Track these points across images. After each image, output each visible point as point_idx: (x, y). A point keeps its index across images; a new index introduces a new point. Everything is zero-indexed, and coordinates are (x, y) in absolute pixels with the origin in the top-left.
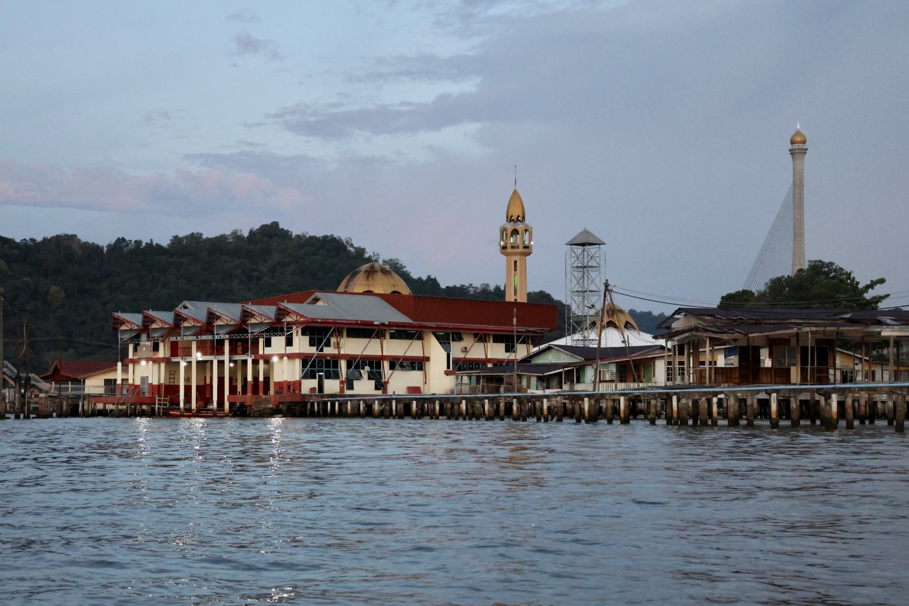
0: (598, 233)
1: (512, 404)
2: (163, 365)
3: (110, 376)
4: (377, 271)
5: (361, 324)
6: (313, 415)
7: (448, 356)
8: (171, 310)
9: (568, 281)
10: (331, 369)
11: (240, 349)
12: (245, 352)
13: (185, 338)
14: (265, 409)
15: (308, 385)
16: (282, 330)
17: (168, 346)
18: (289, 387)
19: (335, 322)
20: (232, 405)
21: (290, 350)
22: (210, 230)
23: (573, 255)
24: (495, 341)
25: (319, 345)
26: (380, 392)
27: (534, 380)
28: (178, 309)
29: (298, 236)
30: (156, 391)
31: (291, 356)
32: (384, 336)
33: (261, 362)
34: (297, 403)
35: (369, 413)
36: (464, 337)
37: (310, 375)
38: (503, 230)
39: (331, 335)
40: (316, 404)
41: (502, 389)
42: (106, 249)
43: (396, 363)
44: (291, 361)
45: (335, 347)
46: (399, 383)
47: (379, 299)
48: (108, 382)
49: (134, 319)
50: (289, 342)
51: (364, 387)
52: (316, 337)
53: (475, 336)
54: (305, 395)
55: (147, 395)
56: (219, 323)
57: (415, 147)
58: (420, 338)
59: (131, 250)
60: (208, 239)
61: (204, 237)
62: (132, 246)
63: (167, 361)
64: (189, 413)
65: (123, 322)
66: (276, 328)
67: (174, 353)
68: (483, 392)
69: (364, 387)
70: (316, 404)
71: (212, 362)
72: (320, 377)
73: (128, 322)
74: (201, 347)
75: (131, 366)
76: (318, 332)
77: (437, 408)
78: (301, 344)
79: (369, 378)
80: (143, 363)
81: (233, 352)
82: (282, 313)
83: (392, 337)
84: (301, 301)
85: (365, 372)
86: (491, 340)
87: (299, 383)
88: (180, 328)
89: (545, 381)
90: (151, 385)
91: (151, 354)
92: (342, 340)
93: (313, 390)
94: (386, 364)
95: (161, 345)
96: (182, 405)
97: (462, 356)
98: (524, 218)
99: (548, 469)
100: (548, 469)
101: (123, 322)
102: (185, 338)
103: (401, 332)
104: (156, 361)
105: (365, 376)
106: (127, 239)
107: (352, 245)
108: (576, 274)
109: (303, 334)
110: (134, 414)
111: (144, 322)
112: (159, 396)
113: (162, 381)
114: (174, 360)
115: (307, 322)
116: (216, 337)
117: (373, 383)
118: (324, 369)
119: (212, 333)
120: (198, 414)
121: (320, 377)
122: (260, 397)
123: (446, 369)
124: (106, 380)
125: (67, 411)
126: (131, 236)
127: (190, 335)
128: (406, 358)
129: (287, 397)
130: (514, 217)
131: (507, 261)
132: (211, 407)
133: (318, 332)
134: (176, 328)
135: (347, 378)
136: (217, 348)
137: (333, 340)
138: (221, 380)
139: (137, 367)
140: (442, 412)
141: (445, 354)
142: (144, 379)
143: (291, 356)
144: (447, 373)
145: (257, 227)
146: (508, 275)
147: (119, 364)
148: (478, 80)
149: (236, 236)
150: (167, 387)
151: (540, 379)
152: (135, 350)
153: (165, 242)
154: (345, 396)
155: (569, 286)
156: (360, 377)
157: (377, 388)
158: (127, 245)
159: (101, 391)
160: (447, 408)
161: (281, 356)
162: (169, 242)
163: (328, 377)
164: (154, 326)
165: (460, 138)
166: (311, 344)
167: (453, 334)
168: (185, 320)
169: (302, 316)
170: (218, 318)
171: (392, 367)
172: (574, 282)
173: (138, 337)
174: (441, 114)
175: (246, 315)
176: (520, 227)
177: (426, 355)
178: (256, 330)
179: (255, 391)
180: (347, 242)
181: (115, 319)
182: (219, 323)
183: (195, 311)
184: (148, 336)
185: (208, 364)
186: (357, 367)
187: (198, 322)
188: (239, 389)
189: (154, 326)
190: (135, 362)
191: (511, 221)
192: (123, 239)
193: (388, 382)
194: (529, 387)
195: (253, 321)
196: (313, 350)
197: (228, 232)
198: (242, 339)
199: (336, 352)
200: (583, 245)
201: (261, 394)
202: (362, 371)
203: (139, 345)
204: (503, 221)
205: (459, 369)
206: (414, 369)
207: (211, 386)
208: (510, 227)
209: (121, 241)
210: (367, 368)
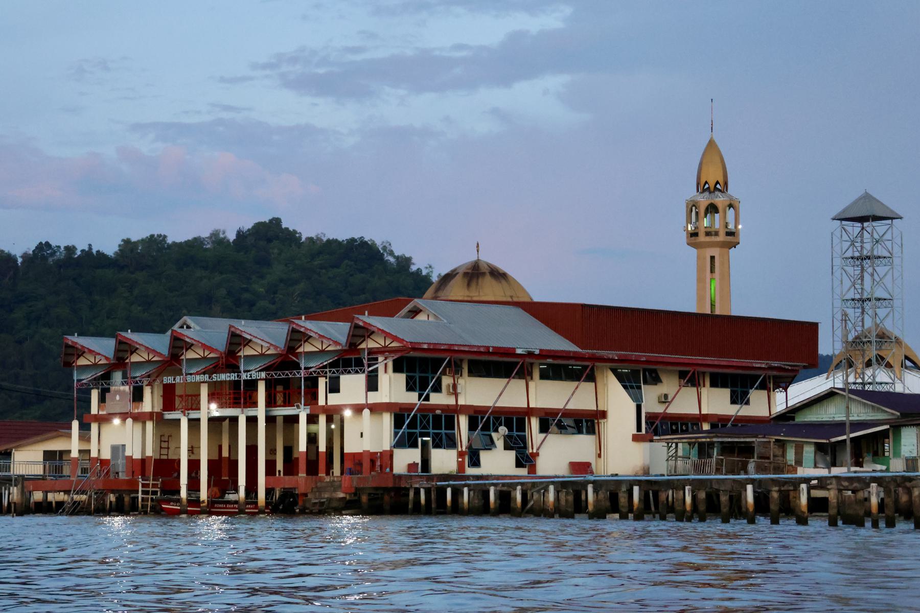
0: (890, 201)
1: (488, 492)
2: (150, 425)
3: (56, 445)
4: (483, 274)
5: (493, 354)
6: (418, 510)
7: (639, 408)
8: (163, 331)
9: (837, 283)
10: (443, 431)
11: (280, 399)
12: (287, 403)
13: (189, 378)
14: (330, 500)
15: (405, 459)
16: (359, 363)
17: (159, 391)
18: (373, 462)
19: (450, 350)
20: (269, 492)
21: (375, 398)
22: (178, 233)
23: (845, 237)
24: (714, 384)
25: (423, 388)
26: (523, 472)
27: (809, 452)
28: (176, 327)
29: (310, 239)
30: (138, 469)
31: (376, 409)
32: (531, 374)
33: (322, 419)
34: (386, 490)
35: (505, 507)
36: (663, 378)
38: (692, 206)
39: (443, 373)
40: (422, 492)
41: (751, 466)
42: (20, 260)
43: (550, 421)
44: (376, 418)
45: (449, 393)
46: (556, 455)
47: (520, 311)
48: (49, 456)
49: (102, 348)
50: (372, 385)
51: (498, 462)
52: (417, 375)
53: (682, 375)
54: (400, 477)
55: (122, 476)
56: (248, 351)
57: (469, 112)
58: (591, 378)
59: (59, 260)
60: (174, 244)
61: (170, 240)
62: (61, 255)
63: (157, 418)
64: (195, 508)
65: (81, 352)
66: (349, 359)
67: (169, 404)
68: (718, 471)
69: (498, 462)
70: (422, 492)
71: (234, 420)
72: (425, 444)
73: (91, 351)
75: (94, 427)
76: (421, 366)
77: (688, 499)
78: (393, 388)
79: (507, 447)
80: (117, 421)
81: (271, 402)
82: (365, 332)
83: (544, 376)
84: (390, 312)
85: (499, 436)
86: (708, 383)
87: (388, 456)
88: (179, 362)
89: (829, 453)
90: (130, 459)
91: (129, 407)
92: (461, 382)
93: (412, 466)
94: (535, 423)
95: (147, 392)
96: (184, 493)
97: (659, 409)
98: (726, 184)
101: (81, 352)
103: (558, 369)
104: (139, 418)
105: (500, 443)
106: (53, 243)
107: (391, 253)
108: (850, 270)
109: (397, 369)
110: (102, 510)
111: (117, 351)
112: (143, 474)
113: (149, 453)
114: (169, 416)
116: (244, 376)
117: (512, 454)
118: (431, 431)
119: (235, 368)
120: (211, 509)
121: (425, 444)
122: (321, 480)
123: (635, 432)
124: (45, 452)
125: (495, 508)
126: (59, 241)
127: (197, 373)
128: (567, 413)
129: (369, 479)
130: (712, 184)
131: (698, 257)
132: (231, 497)
133: (421, 366)
134: (172, 361)
135: (470, 447)
136: (241, 394)
137: (446, 381)
138: (252, 451)
139: (106, 429)
140: (762, 505)
141: (633, 406)
142: (117, 450)
143: (376, 409)
144: (636, 438)
146: (700, 280)
147: (75, 424)
148: (568, 10)
149: (217, 239)
150: (158, 462)
151: (820, 448)
152: (102, 399)
153: (110, 248)
154: (468, 477)
155: (838, 291)
156: (490, 445)
157: (519, 464)
158: (54, 253)
159: (38, 470)
160: (649, 500)
161: (358, 409)
162: (116, 249)
163: (437, 446)
164: (135, 358)
165: (538, 98)
166: (410, 388)
167: (645, 370)
168: (189, 346)
169: (395, 338)
170: (247, 342)
171: (544, 429)
172: (847, 283)
173: (107, 376)
174: (512, 62)
175: (297, 337)
176: (720, 200)
177: (600, 408)
178: (314, 364)
179: (312, 468)
180: (385, 248)
181: (67, 346)
182: (248, 351)
183: (206, 332)
184: (124, 376)
185: (226, 423)
186: (486, 428)
187: (212, 350)
188: (280, 466)
189: (135, 358)
190: (103, 420)
191: (704, 191)
192: (47, 244)
193: (537, 454)
194: (799, 462)
195: (308, 348)
196: (412, 398)
198: (289, 380)
199: (451, 401)
200: (862, 219)
201: (322, 475)
202: (494, 435)
203: (108, 390)
204: (691, 192)
205: (656, 433)
206: (580, 432)
207: (234, 464)
208: (704, 200)
209: (44, 247)
210: (503, 430)
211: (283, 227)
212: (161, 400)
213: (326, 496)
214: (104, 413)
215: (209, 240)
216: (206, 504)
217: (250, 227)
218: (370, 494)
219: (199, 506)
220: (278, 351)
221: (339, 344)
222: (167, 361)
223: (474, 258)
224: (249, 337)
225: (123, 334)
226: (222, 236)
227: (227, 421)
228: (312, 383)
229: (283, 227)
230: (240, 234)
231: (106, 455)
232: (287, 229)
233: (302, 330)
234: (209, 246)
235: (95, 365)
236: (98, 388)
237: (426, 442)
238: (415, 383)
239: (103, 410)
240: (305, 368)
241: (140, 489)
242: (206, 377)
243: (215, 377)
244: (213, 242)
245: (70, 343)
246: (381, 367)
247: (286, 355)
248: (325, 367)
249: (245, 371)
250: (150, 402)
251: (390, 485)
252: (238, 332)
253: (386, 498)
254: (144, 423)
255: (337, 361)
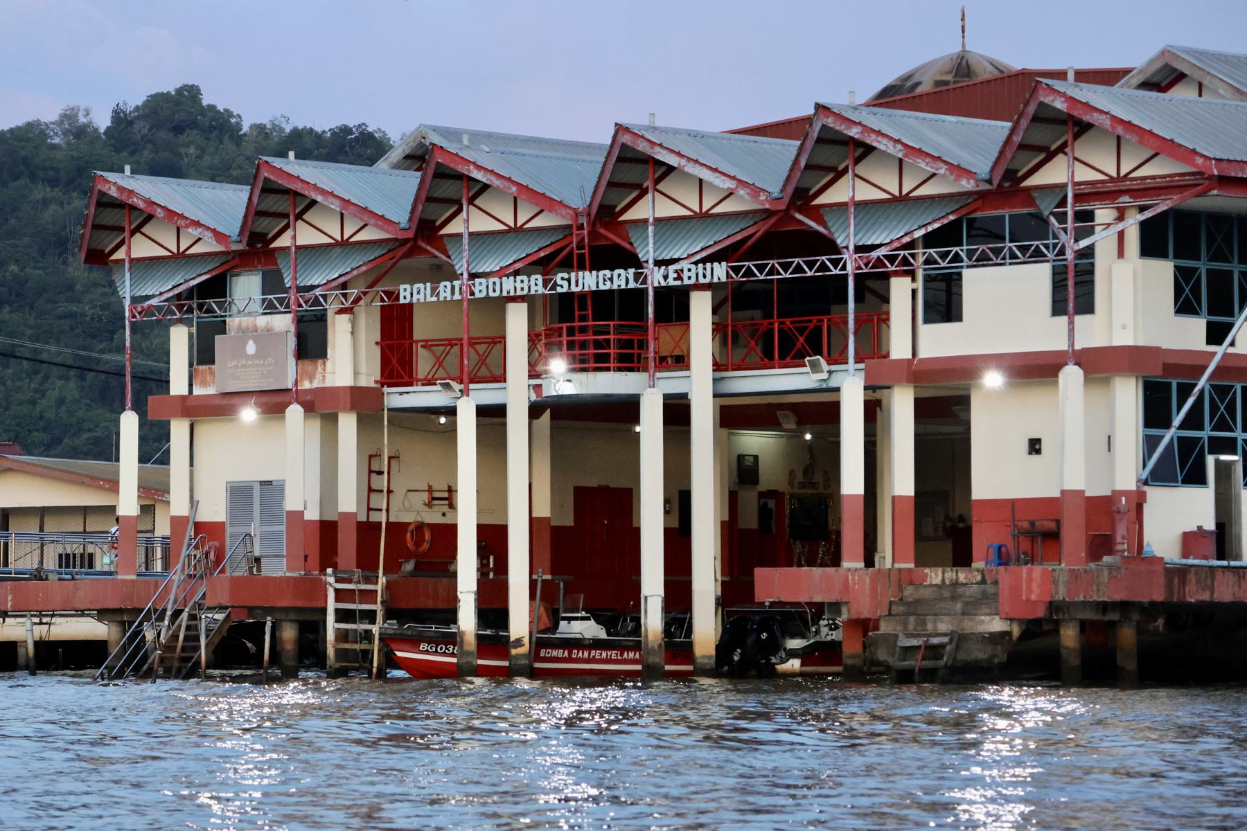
2: (348, 424)
17: (370, 323)
21: (1093, 332)
29: (260, 128)
31: (1100, 364)
37: (1183, 467)
50: (1074, 291)
65: (141, 217)
67: (397, 365)
74: (564, 322)
80: (249, 414)
91: (288, 373)
93: (1190, 541)
95: (339, 330)
96: (467, 620)
99: (494, 785)
100: (494, 785)
101: (141, 217)
102: (481, 289)
109: (1152, 246)
111: (254, 213)
115: (1201, 181)
116: (656, 277)
120: (551, 664)
121: (1224, 471)
127: (501, 273)
143: (1100, 364)
145: (134, 99)
147: (129, 423)
152: (203, 354)
161: (1036, 370)
166: (1185, 307)
169: (1163, 147)
173: (216, 288)
178: (885, 235)
181: (106, 203)
184: (272, 284)
187: (545, 203)
196: (1190, 334)
197: (47, 112)
203: (221, 328)
211: (205, 103)
212: (377, 351)
213: (944, 626)
214: (211, 391)
215: (57, 129)
216: (524, 650)
217: (140, 103)
218: (1084, 626)
219: (505, 655)
220: (762, 203)
221: (969, 173)
222: (406, 241)
223: (954, 48)
224: (673, 160)
225: (277, 162)
226: (82, 120)
227: (547, 414)
228: (873, 289)
229: (205, 103)
230: (120, 118)
231: (214, 510)
232: (212, 108)
233: (854, 132)
234: (57, 140)
235: (179, 258)
236: (188, 323)
237: (1229, 465)
238: (1196, 291)
239: (204, 384)
240: (859, 249)
241: (331, 605)
242: (535, 284)
243: (565, 282)
244: (65, 133)
245: (113, 192)
246: (1103, 241)
247: (786, 215)
248: (911, 245)
249: (658, 263)
250: (350, 357)
251: (1159, 596)
252: (642, 147)
253: (1127, 635)
254: (330, 420)
255: (956, 224)
